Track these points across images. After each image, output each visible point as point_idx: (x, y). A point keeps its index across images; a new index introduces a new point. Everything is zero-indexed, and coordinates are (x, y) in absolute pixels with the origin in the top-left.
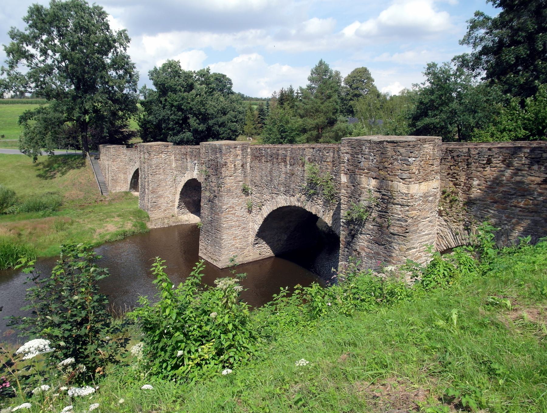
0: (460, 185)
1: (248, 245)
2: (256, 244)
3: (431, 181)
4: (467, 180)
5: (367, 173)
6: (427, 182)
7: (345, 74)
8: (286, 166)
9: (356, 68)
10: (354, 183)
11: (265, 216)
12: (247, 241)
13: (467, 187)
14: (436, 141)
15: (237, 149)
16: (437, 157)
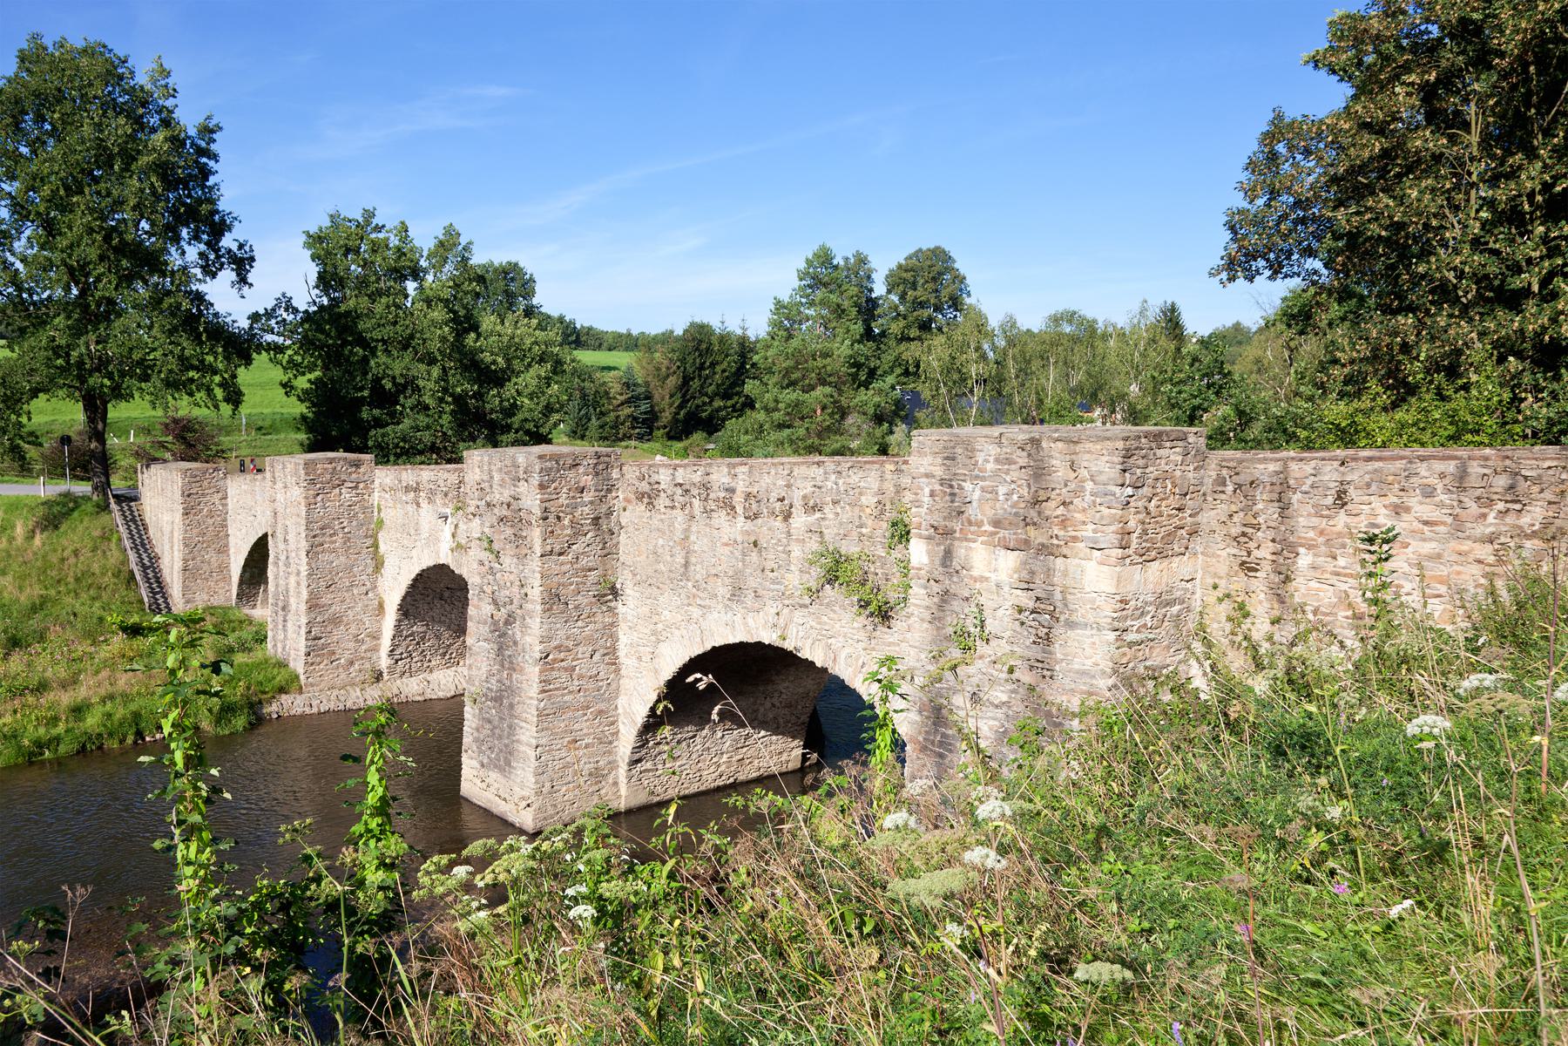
3: (1176, 559)
5: (993, 534)
6: (1166, 561)
7: (882, 266)
15: (581, 470)
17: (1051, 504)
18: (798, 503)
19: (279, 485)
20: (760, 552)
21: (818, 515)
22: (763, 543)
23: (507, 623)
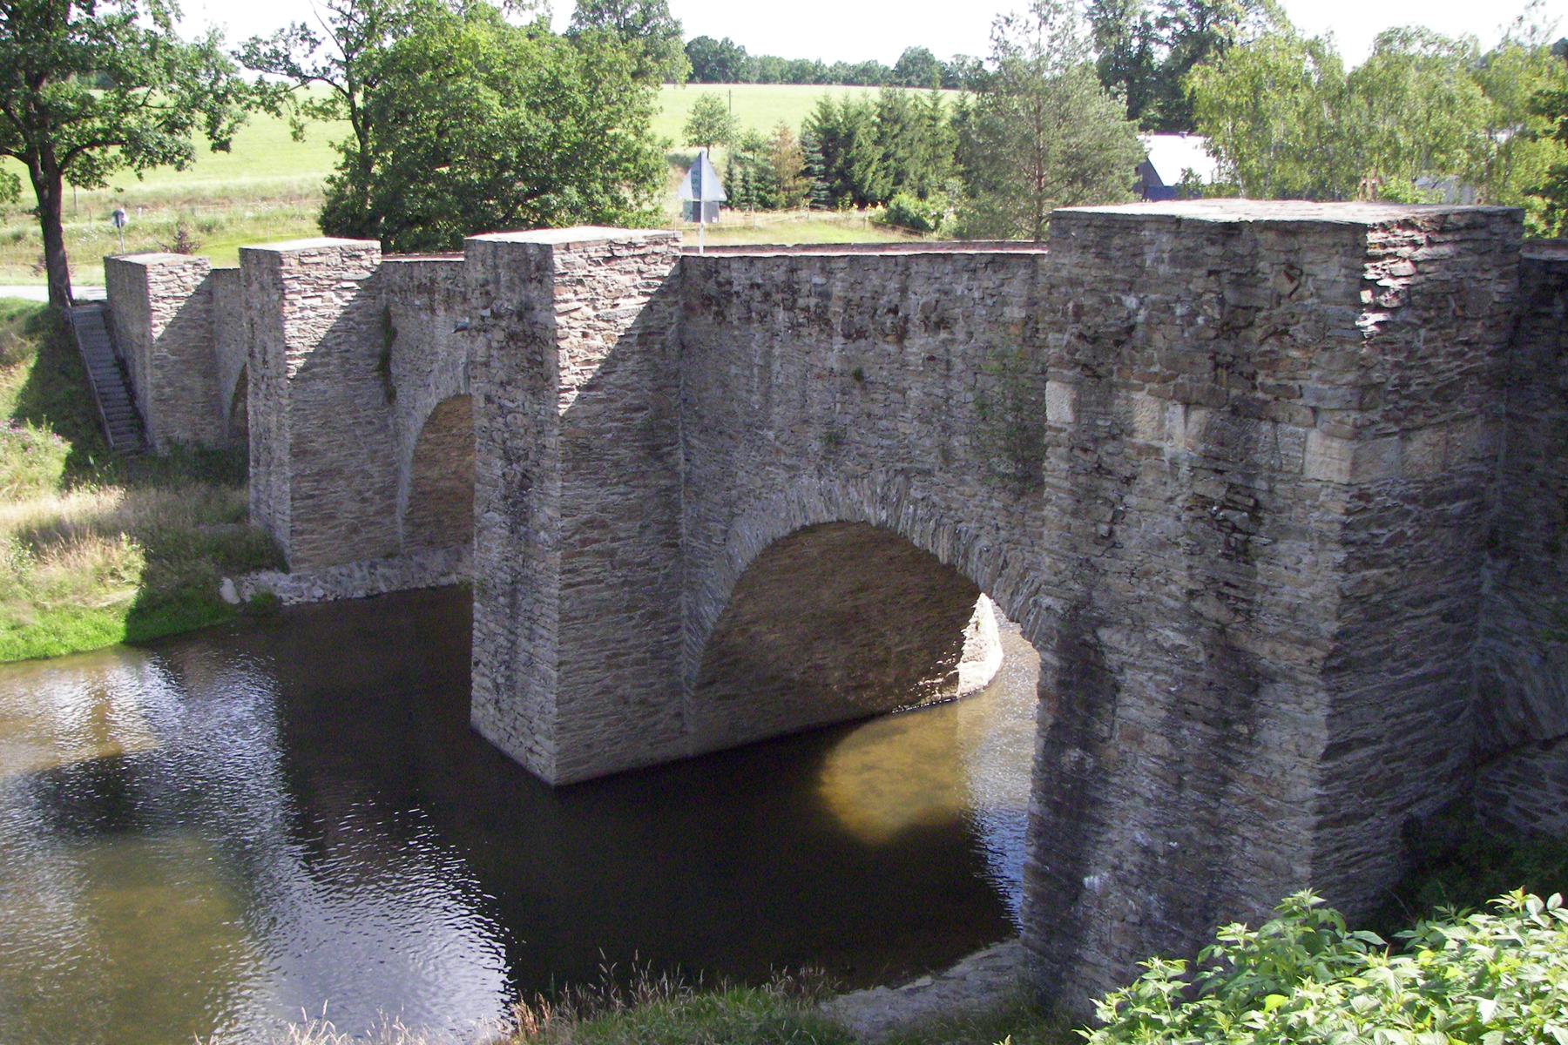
12: (670, 672)
17: (1258, 334)
18: (916, 318)
19: (255, 286)
20: (864, 388)
21: (943, 335)
22: (871, 374)
23: (523, 487)
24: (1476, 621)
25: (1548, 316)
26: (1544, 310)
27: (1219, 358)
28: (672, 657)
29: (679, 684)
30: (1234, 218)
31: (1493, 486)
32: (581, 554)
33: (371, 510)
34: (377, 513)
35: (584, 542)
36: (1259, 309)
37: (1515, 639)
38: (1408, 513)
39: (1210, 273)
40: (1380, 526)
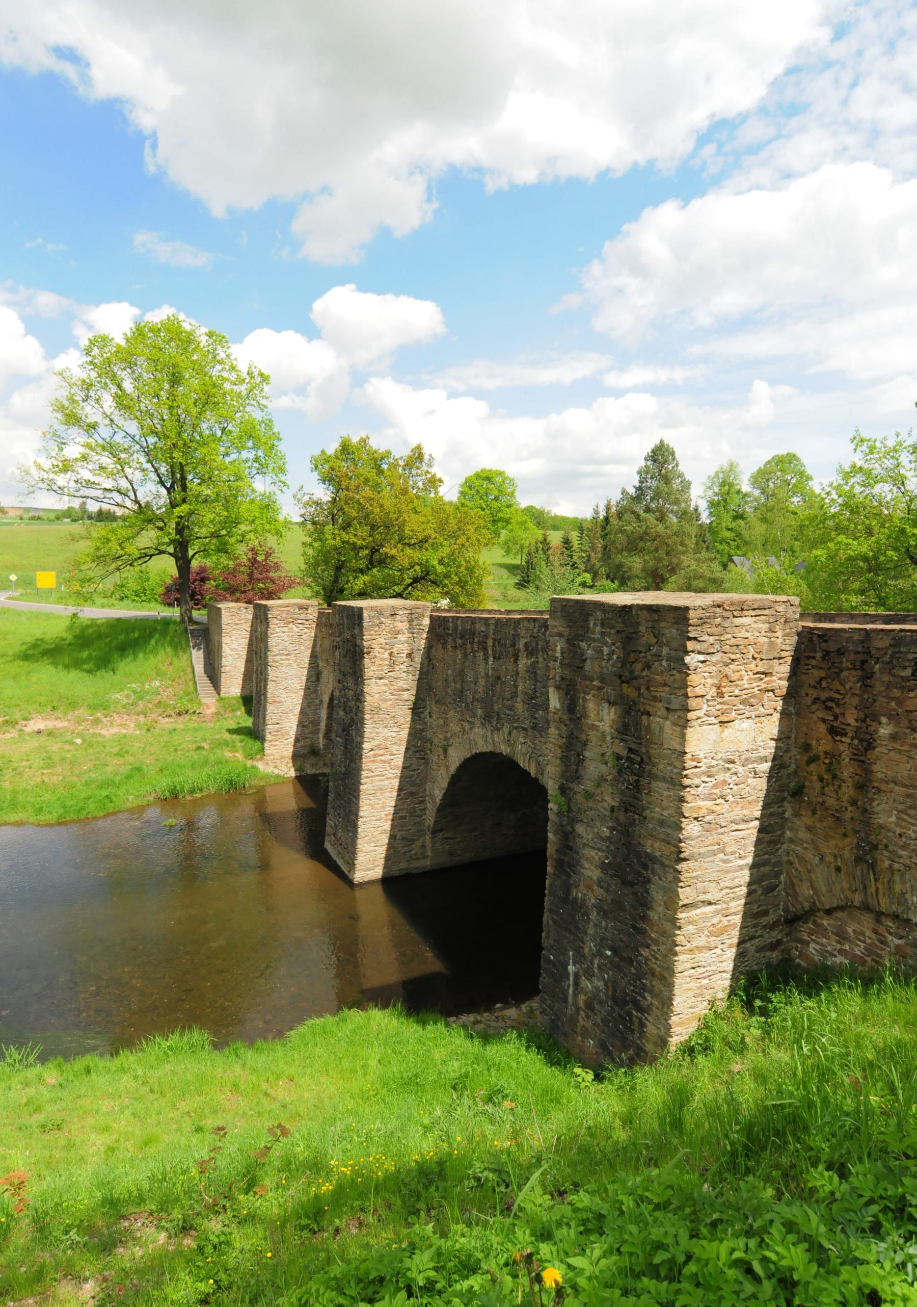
0: (845, 735)
1: (421, 833)
2: (439, 831)
4: (864, 721)
8: (486, 659)
9: (776, 453)
10: (573, 708)
11: (453, 770)
12: (420, 823)
13: (862, 740)
14: (781, 609)
15: (398, 618)
16: (783, 654)
24: (784, 833)
25: (814, 658)
26: (811, 654)
27: (623, 678)
28: (420, 816)
29: (423, 830)
30: (629, 603)
31: (789, 755)
32: (374, 761)
33: (307, 731)
34: (310, 733)
35: (375, 756)
36: (641, 652)
37: (805, 845)
38: (729, 769)
39: (618, 632)
40: (709, 776)
